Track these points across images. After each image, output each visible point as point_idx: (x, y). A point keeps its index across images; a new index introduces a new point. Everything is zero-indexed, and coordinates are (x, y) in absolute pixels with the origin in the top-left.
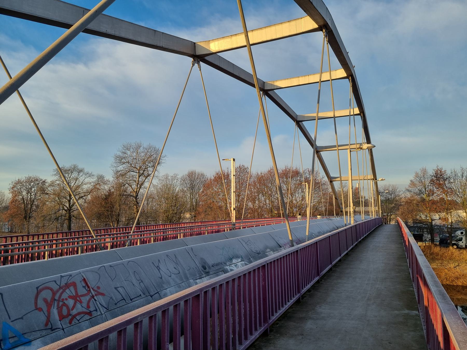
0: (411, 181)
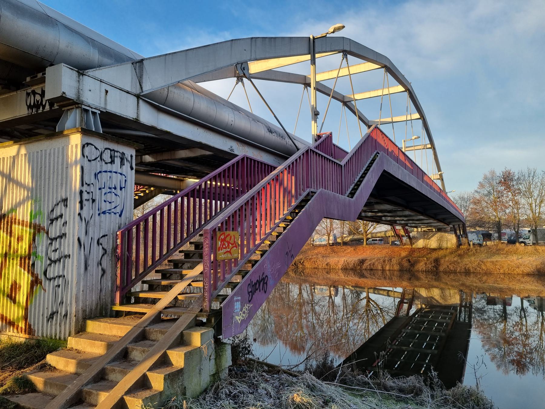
0: (480, 183)
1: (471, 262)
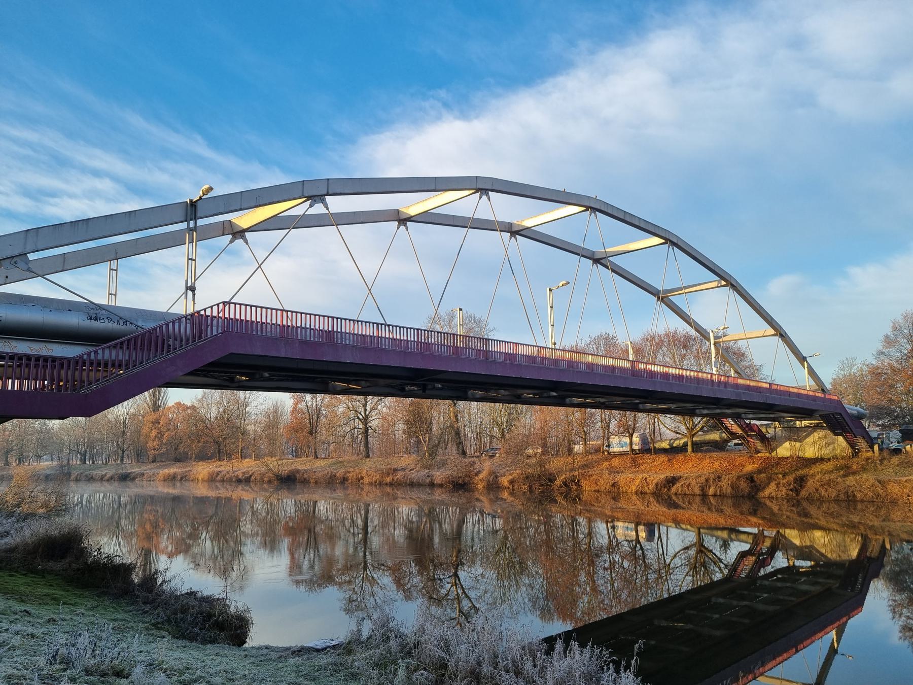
1: (864, 483)
